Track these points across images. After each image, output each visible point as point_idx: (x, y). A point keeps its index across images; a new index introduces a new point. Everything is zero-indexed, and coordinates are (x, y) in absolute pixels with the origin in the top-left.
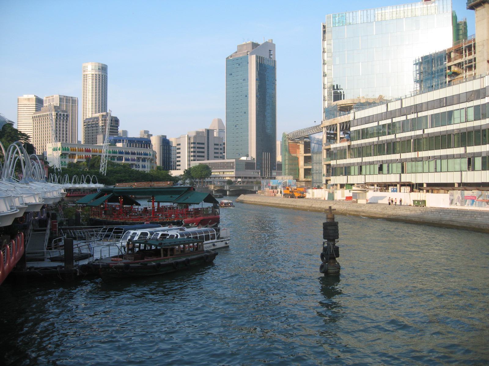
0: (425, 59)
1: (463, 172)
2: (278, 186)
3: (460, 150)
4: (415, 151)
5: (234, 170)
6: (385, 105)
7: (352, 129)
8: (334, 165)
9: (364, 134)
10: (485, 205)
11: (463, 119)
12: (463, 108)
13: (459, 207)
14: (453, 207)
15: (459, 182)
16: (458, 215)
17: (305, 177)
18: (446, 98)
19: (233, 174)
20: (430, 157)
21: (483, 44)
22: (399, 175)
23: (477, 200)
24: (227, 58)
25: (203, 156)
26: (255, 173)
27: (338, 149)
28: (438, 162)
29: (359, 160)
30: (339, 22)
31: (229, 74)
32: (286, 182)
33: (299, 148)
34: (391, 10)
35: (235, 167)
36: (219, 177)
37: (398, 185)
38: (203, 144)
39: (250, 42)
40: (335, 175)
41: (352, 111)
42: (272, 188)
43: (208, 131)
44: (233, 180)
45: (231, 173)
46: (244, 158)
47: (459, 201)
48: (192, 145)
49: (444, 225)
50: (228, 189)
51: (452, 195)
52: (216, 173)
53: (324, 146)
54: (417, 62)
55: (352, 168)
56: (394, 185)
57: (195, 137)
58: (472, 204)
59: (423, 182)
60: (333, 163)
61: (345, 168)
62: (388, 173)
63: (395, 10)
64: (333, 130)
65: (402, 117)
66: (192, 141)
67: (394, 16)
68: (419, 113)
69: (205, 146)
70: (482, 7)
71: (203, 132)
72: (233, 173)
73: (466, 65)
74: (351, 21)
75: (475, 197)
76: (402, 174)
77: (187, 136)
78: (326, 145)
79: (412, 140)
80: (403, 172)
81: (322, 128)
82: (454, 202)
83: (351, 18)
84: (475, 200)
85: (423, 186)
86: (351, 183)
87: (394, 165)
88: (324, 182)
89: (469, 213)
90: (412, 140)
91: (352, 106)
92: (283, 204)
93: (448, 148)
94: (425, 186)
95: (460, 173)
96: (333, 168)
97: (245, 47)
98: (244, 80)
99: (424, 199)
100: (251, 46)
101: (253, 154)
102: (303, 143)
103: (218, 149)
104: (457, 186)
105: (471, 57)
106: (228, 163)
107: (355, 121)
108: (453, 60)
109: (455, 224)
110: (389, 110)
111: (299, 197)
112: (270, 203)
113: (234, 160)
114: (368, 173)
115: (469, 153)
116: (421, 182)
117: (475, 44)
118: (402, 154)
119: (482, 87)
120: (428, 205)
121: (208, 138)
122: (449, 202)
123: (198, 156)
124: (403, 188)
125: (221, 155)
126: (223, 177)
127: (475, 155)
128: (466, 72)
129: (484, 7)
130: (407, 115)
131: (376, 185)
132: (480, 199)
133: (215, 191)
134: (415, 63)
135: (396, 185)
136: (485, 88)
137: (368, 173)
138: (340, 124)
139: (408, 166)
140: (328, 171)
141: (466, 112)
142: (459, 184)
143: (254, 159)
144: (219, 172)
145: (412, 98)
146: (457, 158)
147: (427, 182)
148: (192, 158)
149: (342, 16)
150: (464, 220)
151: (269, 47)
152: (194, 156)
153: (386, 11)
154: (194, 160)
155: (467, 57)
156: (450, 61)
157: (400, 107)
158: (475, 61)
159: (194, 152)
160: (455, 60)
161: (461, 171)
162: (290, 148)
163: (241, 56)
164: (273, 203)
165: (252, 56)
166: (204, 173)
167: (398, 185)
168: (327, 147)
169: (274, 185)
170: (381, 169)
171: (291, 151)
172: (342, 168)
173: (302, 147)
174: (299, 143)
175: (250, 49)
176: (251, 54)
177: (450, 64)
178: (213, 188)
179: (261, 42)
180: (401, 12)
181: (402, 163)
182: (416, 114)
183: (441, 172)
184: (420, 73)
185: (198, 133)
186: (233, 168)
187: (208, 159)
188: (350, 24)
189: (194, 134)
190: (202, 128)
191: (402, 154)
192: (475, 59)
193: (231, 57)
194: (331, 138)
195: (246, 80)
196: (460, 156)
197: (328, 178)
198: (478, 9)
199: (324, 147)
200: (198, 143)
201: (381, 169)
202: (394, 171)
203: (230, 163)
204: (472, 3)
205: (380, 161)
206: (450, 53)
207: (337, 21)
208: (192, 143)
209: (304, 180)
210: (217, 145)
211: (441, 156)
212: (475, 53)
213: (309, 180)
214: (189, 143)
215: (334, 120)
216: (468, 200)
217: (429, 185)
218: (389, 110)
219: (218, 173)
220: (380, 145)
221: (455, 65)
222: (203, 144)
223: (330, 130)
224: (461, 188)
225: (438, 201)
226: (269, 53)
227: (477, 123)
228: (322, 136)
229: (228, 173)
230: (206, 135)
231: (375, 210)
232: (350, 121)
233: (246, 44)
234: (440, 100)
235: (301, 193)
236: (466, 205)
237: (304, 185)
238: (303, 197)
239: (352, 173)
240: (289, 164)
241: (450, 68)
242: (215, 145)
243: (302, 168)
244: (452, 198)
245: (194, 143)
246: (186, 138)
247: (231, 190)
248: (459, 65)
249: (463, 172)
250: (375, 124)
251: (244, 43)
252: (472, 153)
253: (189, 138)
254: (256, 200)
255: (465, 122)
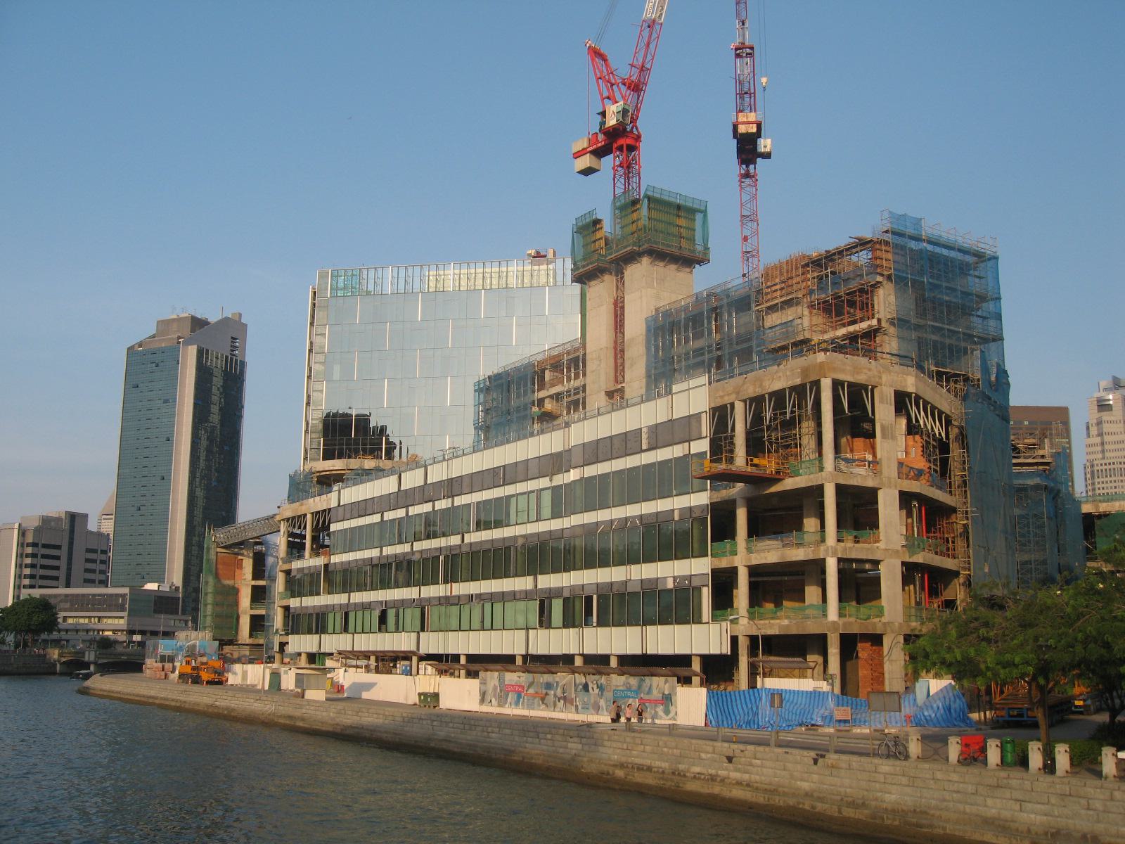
0: (495, 381)
1: (530, 631)
2: (177, 655)
3: (523, 583)
4: (446, 582)
5: (125, 614)
6: (396, 476)
7: (333, 527)
8: (295, 608)
9: (354, 540)
10: (539, 705)
11: (533, 516)
12: (533, 492)
13: (494, 709)
14: (485, 708)
15: (524, 652)
16: (462, 726)
17: (251, 636)
18: (504, 466)
19: (122, 623)
20: (472, 595)
21: (599, 357)
22: (415, 634)
23: (526, 694)
24: (130, 349)
25: (56, 578)
26: (177, 622)
27: (306, 571)
28: (488, 606)
29: (341, 599)
30: (344, 288)
31: (133, 385)
32: (194, 646)
33: (241, 567)
34: (520, 268)
35: (127, 606)
36: (87, 631)
37: (415, 659)
38: (59, 547)
39: (186, 315)
40: (297, 633)
41: (336, 488)
42: (163, 659)
43: (73, 517)
44: (122, 637)
45: (116, 621)
46: (152, 586)
47: (495, 696)
48: (29, 550)
49: (433, 749)
50: (92, 658)
51: (483, 683)
52: (82, 621)
53: (281, 563)
54: (482, 386)
55: (331, 616)
56: (406, 656)
57: (37, 531)
58: (517, 703)
59: (515, 653)
60: (294, 603)
61: (317, 615)
62: (397, 630)
63: (464, 271)
64: (300, 527)
65: (425, 505)
66: (30, 539)
67: (526, 281)
68: (455, 498)
69: (64, 553)
70: (599, 280)
71: (59, 519)
72: (122, 621)
73: (570, 399)
74: (371, 288)
75: (523, 687)
76: (421, 633)
77: (17, 526)
78: (284, 562)
79: (442, 558)
80: (423, 629)
81: (280, 521)
82: (488, 698)
83: (417, 281)
84: (523, 694)
85: (608, 663)
86: (327, 651)
87: (408, 611)
88: (277, 648)
89: (481, 723)
90: (442, 558)
91: (344, 474)
92: (162, 698)
93: (507, 576)
94: (463, 660)
95: (524, 631)
96: (293, 616)
97: (175, 326)
98: (166, 401)
99: (436, 691)
100: (189, 324)
101: (175, 576)
102: (251, 555)
103: (94, 561)
104: (521, 664)
105: (578, 383)
106: (111, 595)
107: (341, 510)
108: (547, 386)
109: (451, 747)
110: (402, 489)
111: (209, 683)
112: (137, 696)
113: (126, 590)
114: (359, 629)
115: (542, 589)
116: (510, 652)
117: (584, 355)
118: (422, 588)
119: (567, 448)
120: (446, 703)
121: (72, 531)
122: (478, 697)
123: (42, 577)
124: (422, 665)
125: (102, 577)
126: (99, 631)
127: (552, 594)
128: (568, 413)
129: (603, 281)
130: (433, 501)
131: (373, 658)
132: (531, 691)
133: (61, 664)
134: (477, 388)
135: (368, 658)
136: (570, 450)
137: (359, 629)
138: (312, 513)
139: (433, 614)
140: (286, 624)
141: (538, 499)
142: (525, 657)
143: (177, 588)
144: (90, 617)
145: (445, 463)
146: (520, 600)
147: (623, 652)
148: (27, 582)
149: (353, 275)
150: (469, 738)
151: (233, 331)
152: (32, 577)
153: (510, 269)
154: (31, 587)
155: (572, 381)
156: (541, 388)
157: (422, 484)
158: (584, 391)
159: (33, 566)
160: (553, 385)
161: (527, 629)
162: (220, 567)
163: (163, 345)
164: (144, 696)
165: (190, 347)
166: (36, 619)
167: (415, 659)
168: (286, 567)
169: (168, 653)
170: (383, 619)
171: (220, 572)
172: (311, 615)
173: (248, 564)
174: (242, 555)
175: (186, 330)
176: (187, 343)
177: (542, 394)
178: (56, 657)
179: (213, 318)
180: (542, 273)
181: (422, 606)
182: (450, 500)
183: (470, 630)
184: (487, 411)
185: (46, 521)
186: (123, 609)
187: (68, 585)
188: (368, 293)
189: (36, 523)
190: (57, 508)
191: (422, 588)
192: (584, 386)
193: (140, 346)
194: (296, 548)
195: (170, 401)
196: (526, 596)
197: (284, 639)
198: (592, 283)
199: (282, 566)
200: (45, 546)
201: (383, 619)
202: (408, 627)
203: (117, 595)
204: (581, 270)
205: (382, 602)
206: (543, 371)
207: (341, 285)
208: (28, 545)
209: (248, 641)
210: (94, 551)
211: (491, 594)
212: (584, 375)
213: (261, 641)
214: (21, 545)
215: (302, 505)
216: (510, 693)
217: (472, 658)
218: (402, 489)
219: (87, 621)
220: (383, 566)
221: (551, 397)
222: (59, 547)
223: (294, 527)
224: (591, 668)
225: (460, 695)
226: (229, 344)
227: (556, 524)
228: (280, 541)
229: (110, 621)
230: (65, 526)
231: (324, 714)
232: (330, 509)
233: (179, 320)
234: (494, 470)
235: (216, 672)
236: (507, 706)
237: (247, 653)
238: (220, 683)
239: (330, 629)
240: (216, 604)
241: (541, 402)
242: (89, 550)
243: (245, 613)
244: (483, 688)
245: (34, 545)
246: (16, 532)
247: (100, 661)
248: (557, 397)
249: (530, 631)
250: (376, 518)
251: (174, 316)
252: (547, 589)
253: (22, 533)
254: (114, 688)
255: (537, 521)
